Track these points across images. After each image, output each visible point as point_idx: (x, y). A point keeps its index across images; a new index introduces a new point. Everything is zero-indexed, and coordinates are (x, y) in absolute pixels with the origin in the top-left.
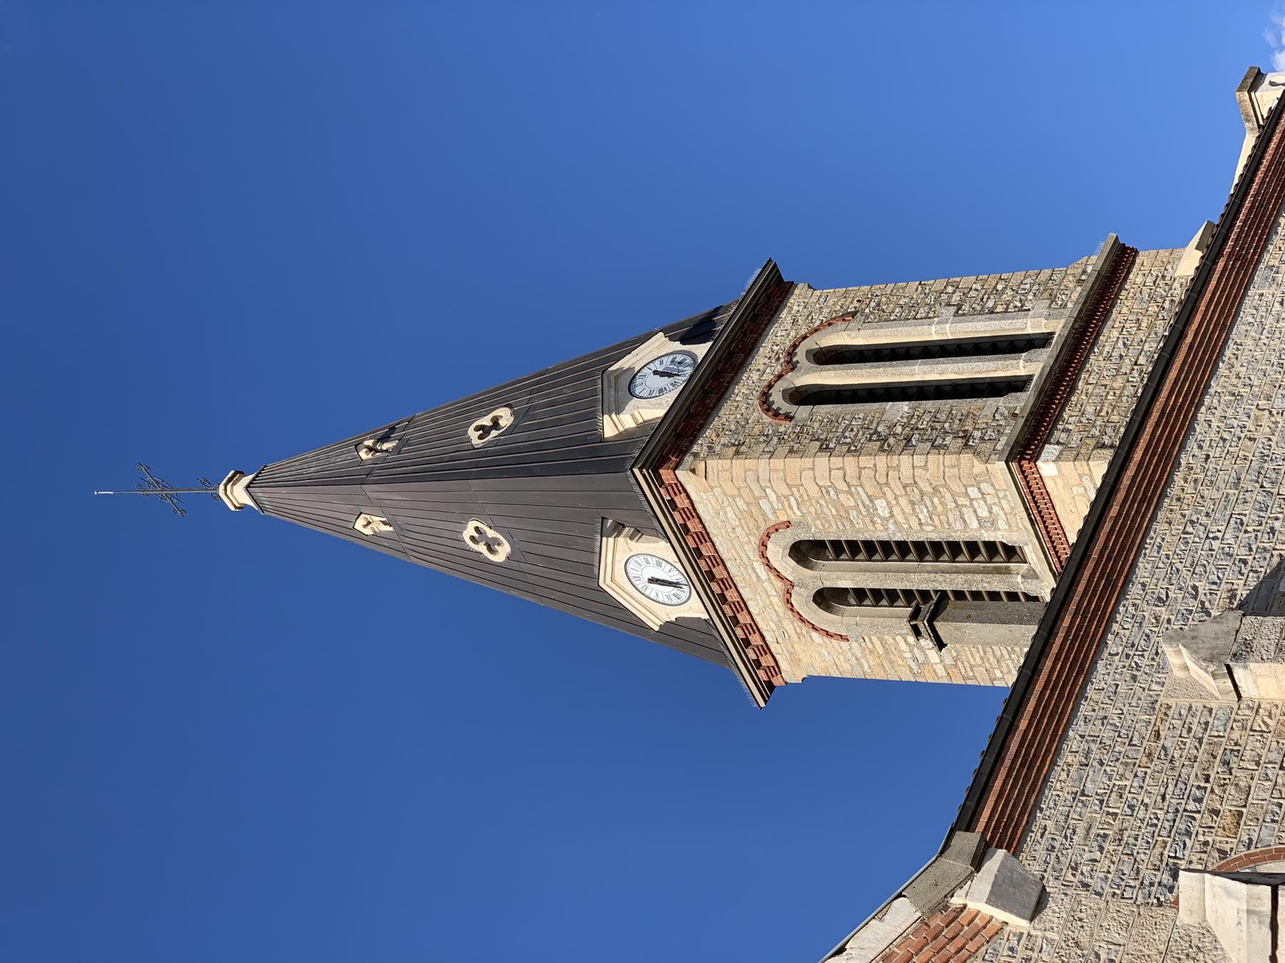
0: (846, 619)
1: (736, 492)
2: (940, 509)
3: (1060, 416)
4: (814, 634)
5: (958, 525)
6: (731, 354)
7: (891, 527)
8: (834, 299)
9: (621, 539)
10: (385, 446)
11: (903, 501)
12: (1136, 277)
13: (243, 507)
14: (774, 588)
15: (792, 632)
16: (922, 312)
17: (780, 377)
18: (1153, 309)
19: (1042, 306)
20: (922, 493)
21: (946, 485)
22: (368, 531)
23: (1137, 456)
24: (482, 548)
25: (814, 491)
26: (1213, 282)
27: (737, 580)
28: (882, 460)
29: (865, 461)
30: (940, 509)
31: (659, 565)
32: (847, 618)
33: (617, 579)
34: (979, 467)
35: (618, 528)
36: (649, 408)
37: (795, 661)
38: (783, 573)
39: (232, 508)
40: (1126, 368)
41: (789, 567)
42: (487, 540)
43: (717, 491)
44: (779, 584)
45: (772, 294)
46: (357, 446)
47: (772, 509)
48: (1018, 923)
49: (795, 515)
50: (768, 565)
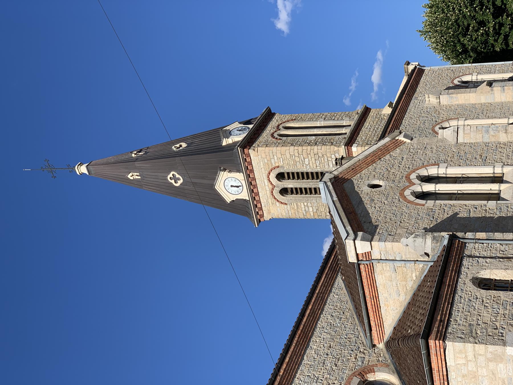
0: (287, 198)
1: (265, 158)
2: (323, 161)
3: (356, 139)
4: (277, 203)
5: (327, 167)
6: (260, 126)
7: (308, 167)
8: (288, 117)
9: (226, 172)
10: (140, 154)
11: (313, 159)
12: (371, 114)
13: (82, 174)
14: (268, 187)
15: (270, 203)
16: (314, 119)
17: (276, 131)
18: (377, 119)
19: (348, 118)
20: (319, 157)
21: (326, 154)
22: (132, 178)
23: (391, 126)
24: (173, 181)
25: (288, 156)
26: (403, 99)
27: (258, 186)
28: (309, 147)
29: (304, 148)
30: (323, 161)
31: (235, 181)
32: (289, 198)
33: (220, 186)
34: (336, 148)
35: (225, 170)
36: (238, 138)
37: (269, 212)
38: (273, 183)
39: (78, 174)
40: (372, 130)
41: (274, 181)
42: (176, 179)
43: (260, 156)
44: (271, 186)
45: (269, 116)
46: (131, 152)
47: (275, 162)
48: (408, 141)
49: (281, 164)
50: (269, 180)
